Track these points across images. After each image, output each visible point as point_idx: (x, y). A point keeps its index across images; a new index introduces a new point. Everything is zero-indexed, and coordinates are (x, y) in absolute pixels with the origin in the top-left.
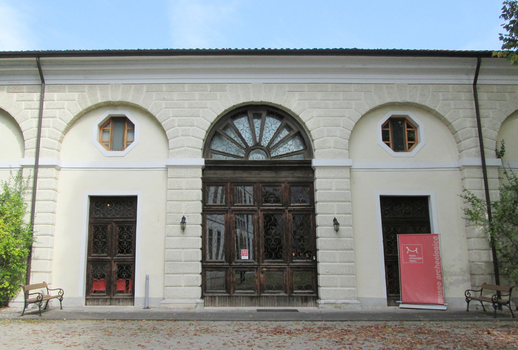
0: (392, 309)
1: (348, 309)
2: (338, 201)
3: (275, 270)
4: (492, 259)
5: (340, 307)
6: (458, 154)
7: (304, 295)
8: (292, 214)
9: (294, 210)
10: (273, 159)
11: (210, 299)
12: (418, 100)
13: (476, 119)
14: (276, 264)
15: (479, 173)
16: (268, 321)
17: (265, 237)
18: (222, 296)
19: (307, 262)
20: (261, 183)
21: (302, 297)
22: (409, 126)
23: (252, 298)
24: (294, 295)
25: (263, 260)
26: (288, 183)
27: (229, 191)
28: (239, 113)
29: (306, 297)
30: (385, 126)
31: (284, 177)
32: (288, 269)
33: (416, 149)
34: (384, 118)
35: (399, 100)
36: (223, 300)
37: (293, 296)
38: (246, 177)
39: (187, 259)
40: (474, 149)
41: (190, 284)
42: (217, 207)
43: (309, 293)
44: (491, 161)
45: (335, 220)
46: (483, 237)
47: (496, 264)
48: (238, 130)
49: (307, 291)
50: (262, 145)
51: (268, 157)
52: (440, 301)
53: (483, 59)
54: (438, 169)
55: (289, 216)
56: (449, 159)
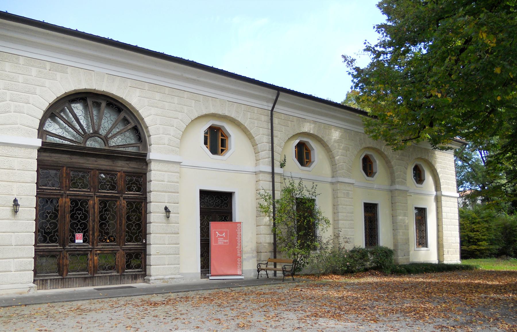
0: (205, 280)
1: (173, 283)
2: (169, 192)
3: (109, 252)
4: (272, 241)
5: (167, 282)
6: (255, 162)
7: (134, 273)
8: (127, 202)
9: (128, 198)
10: (111, 149)
11: (41, 282)
12: (233, 115)
13: (270, 137)
14: (110, 247)
15: (269, 177)
16: (172, 293)
17: (100, 222)
18: (54, 279)
19: (138, 245)
20: (98, 170)
21: (132, 275)
22: (222, 135)
23: (85, 278)
24: (125, 274)
25: (97, 243)
26: (124, 172)
27: (64, 175)
28: (77, 99)
29: (136, 275)
30: (206, 133)
31: (121, 167)
32: (121, 251)
33: (228, 155)
34: (205, 126)
35: (220, 112)
36: (55, 283)
37: (124, 275)
38: (83, 163)
39: (19, 243)
40: (267, 159)
41: (22, 268)
42: (51, 191)
43: (138, 271)
44: (278, 170)
45: (166, 208)
46: (268, 225)
47: (275, 244)
48: (76, 115)
49: (137, 270)
50: (101, 133)
51: (105, 145)
52: (239, 272)
53: (281, 93)
54: (240, 173)
55: (123, 203)
56: (249, 165)
